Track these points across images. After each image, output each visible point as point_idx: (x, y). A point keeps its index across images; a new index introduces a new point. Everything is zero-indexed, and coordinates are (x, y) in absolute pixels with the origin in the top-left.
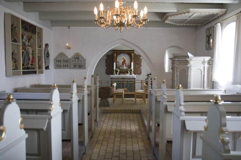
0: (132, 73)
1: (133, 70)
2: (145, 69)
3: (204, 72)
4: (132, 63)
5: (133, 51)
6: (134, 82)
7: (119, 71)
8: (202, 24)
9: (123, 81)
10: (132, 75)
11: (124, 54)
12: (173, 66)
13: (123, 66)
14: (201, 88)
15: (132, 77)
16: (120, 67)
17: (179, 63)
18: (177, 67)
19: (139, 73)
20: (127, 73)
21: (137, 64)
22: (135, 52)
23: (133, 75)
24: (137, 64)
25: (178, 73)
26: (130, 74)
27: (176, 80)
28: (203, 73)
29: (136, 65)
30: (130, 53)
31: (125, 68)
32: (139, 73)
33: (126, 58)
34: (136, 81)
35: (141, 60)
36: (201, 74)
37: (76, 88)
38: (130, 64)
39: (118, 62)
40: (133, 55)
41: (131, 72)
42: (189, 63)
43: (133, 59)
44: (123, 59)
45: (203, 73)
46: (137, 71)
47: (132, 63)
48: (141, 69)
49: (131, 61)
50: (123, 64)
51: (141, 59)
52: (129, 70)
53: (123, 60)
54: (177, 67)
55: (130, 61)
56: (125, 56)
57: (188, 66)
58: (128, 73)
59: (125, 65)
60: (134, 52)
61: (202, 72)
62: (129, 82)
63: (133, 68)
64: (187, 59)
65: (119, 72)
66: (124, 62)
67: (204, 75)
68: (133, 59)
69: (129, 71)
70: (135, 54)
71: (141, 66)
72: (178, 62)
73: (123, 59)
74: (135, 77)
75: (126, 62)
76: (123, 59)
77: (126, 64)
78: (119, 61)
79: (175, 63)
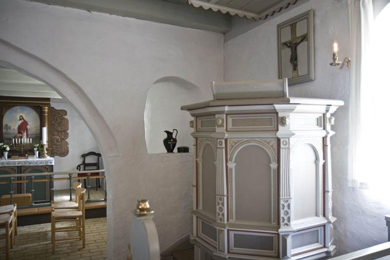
0: (44, 154)
1: (46, 147)
2: (80, 139)
3: (325, 158)
4: (45, 130)
5: (48, 99)
6: (51, 177)
7: (8, 149)
8: (259, 13)
9: (20, 178)
10: (44, 157)
11: (24, 107)
12: (198, 134)
13: (21, 138)
14: (317, 215)
15: (45, 164)
16: (11, 140)
17: (234, 123)
18: (226, 140)
19: (64, 153)
20: (32, 153)
21: (57, 131)
22: (53, 105)
23: (48, 158)
24: (57, 131)
25: (232, 165)
26: (39, 157)
27: (225, 193)
28: (321, 162)
29: (56, 133)
30: (38, 105)
31: (25, 140)
32: (64, 153)
33: (31, 117)
34: (55, 177)
35: (68, 123)
36: (314, 166)
37: (298, 64)
38: (38, 131)
39: (6, 125)
40: (46, 109)
41: (43, 150)
42: (283, 121)
43: (46, 118)
44: (20, 119)
45: (321, 162)
46: (58, 148)
47: (45, 130)
48: (67, 143)
49: (42, 125)
50: (19, 132)
51: (67, 120)
52: (38, 145)
53: (20, 122)
54: (226, 140)
55: (39, 124)
56: (25, 112)
57: (279, 134)
58: (34, 154)
59: (25, 134)
60: (49, 104)
61: (317, 159)
62: (35, 179)
63: (48, 142)
64: (277, 107)
65: (9, 151)
66: (23, 127)
67: (324, 166)
68: (46, 118)
69: (35, 149)
70: (52, 110)
71: (67, 135)
72: (230, 120)
73: (20, 119)
74: (53, 164)
75: (28, 127)
76: (21, 118)
77: (29, 133)
78: (9, 125)
79: (222, 126)
